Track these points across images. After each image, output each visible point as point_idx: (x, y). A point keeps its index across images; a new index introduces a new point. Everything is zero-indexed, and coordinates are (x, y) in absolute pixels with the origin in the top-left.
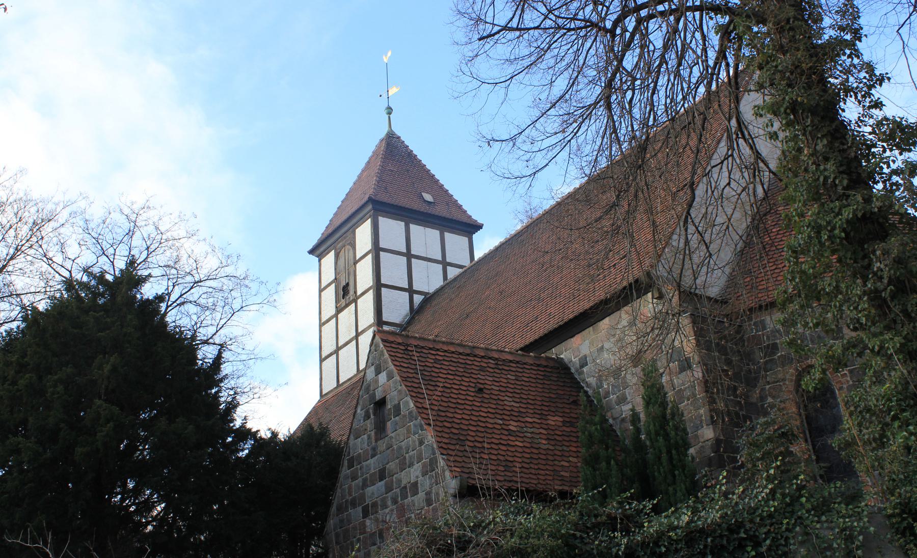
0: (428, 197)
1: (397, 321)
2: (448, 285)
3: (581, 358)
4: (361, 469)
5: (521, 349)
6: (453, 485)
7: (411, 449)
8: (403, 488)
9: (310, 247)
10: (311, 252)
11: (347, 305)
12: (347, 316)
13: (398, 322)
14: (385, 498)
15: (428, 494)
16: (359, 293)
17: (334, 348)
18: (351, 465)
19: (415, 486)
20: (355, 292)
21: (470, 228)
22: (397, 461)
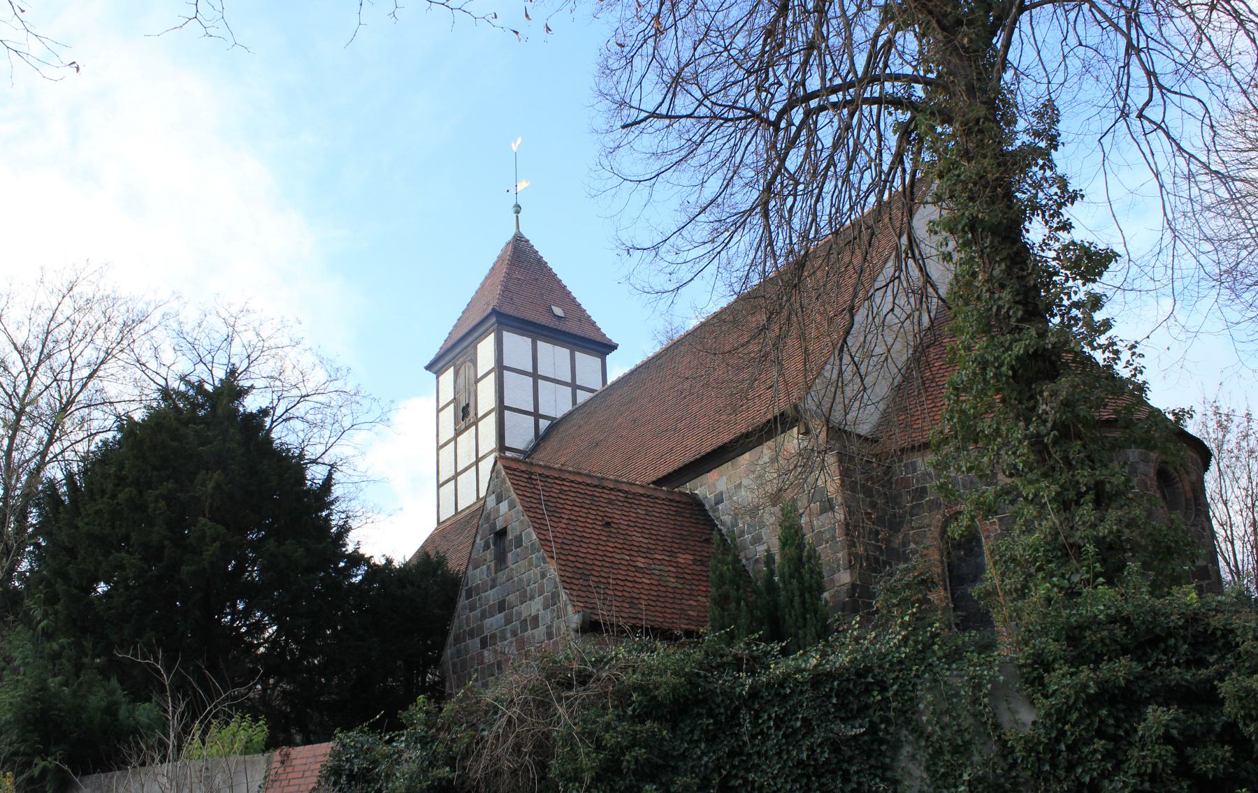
0: (558, 311)
1: (521, 447)
2: (577, 410)
5: (654, 483)
9: (427, 363)
10: (428, 368)
11: (467, 428)
12: (467, 439)
15: (549, 627)
16: (479, 416)
17: (453, 473)
18: (469, 596)
19: (535, 620)
21: (603, 347)
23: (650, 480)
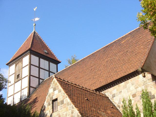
0: (46, 52)
3: (113, 95)
5: (95, 90)
9: (7, 63)
11: (18, 81)
16: (23, 77)
20: (22, 66)
21: (57, 62)
23: (94, 89)
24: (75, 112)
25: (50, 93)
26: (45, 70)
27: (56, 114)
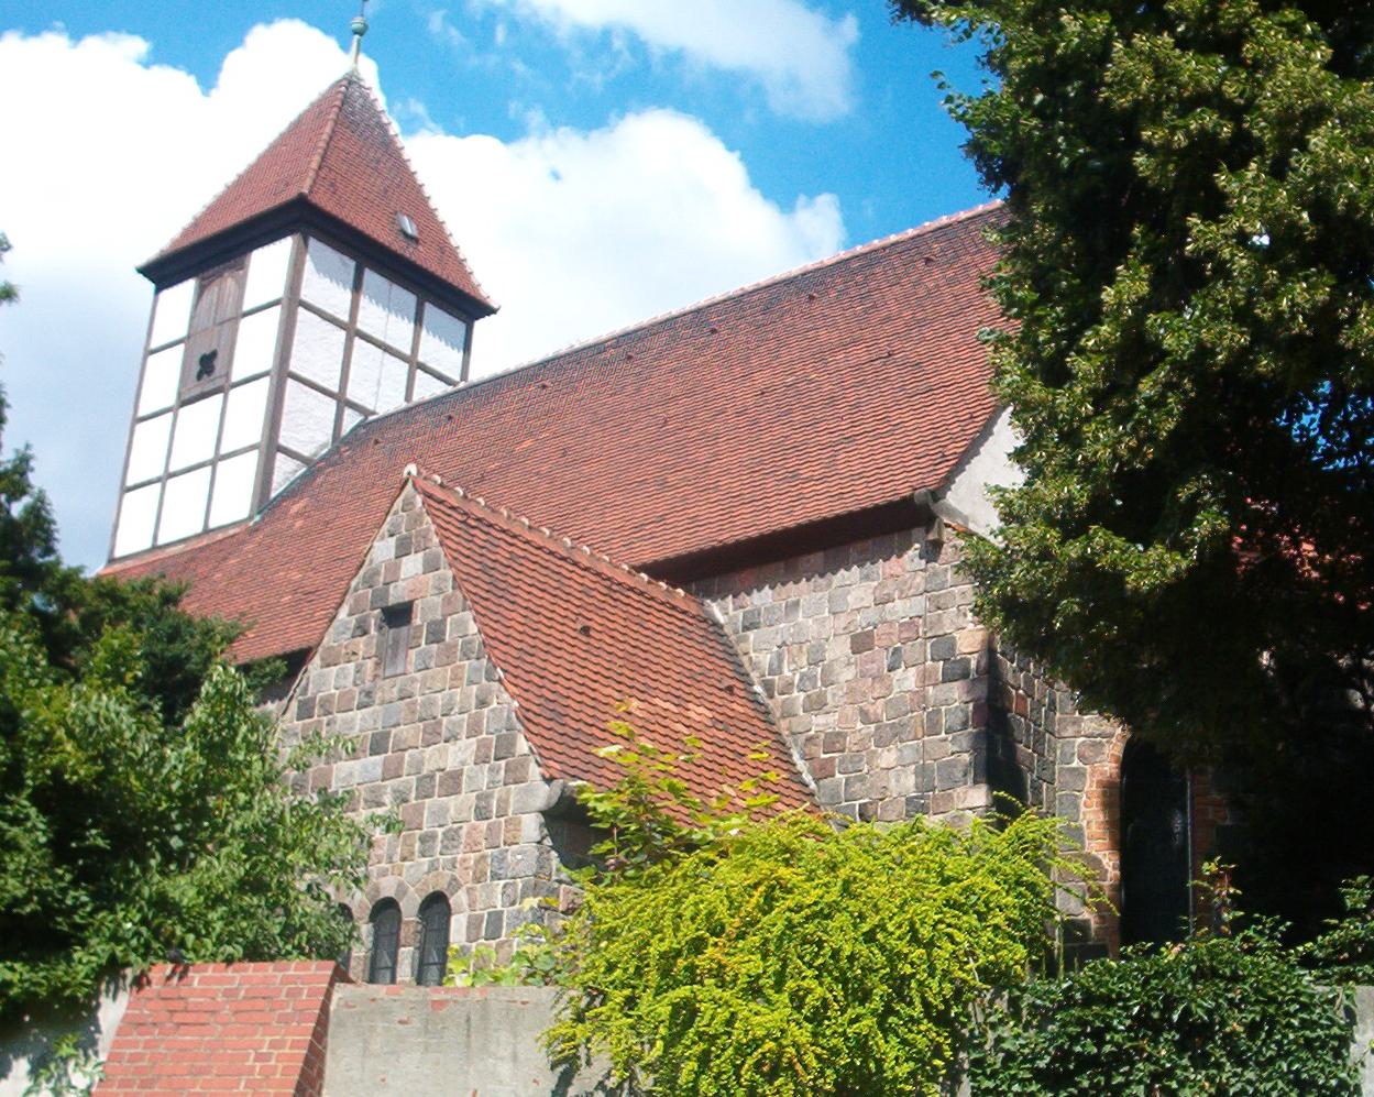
0: (410, 229)
1: (306, 452)
4: (328, 724)
5: (657, 570)
6: (544, 795)
7: (456, 710)
8: (426, 777)
13: (306, 454)
14: (380, 787)
15: (483, 798)
19: (452, 782)
20: (228, 375)
21: (467, 307)
22: (421, 725)
24: (495, 700)
25: (376, 562)
26: (387, 349)
27: (395, 690)
